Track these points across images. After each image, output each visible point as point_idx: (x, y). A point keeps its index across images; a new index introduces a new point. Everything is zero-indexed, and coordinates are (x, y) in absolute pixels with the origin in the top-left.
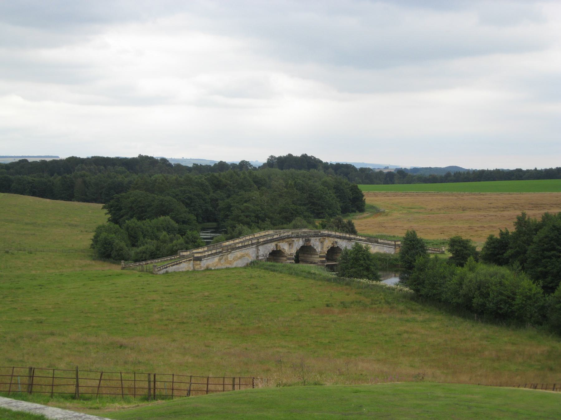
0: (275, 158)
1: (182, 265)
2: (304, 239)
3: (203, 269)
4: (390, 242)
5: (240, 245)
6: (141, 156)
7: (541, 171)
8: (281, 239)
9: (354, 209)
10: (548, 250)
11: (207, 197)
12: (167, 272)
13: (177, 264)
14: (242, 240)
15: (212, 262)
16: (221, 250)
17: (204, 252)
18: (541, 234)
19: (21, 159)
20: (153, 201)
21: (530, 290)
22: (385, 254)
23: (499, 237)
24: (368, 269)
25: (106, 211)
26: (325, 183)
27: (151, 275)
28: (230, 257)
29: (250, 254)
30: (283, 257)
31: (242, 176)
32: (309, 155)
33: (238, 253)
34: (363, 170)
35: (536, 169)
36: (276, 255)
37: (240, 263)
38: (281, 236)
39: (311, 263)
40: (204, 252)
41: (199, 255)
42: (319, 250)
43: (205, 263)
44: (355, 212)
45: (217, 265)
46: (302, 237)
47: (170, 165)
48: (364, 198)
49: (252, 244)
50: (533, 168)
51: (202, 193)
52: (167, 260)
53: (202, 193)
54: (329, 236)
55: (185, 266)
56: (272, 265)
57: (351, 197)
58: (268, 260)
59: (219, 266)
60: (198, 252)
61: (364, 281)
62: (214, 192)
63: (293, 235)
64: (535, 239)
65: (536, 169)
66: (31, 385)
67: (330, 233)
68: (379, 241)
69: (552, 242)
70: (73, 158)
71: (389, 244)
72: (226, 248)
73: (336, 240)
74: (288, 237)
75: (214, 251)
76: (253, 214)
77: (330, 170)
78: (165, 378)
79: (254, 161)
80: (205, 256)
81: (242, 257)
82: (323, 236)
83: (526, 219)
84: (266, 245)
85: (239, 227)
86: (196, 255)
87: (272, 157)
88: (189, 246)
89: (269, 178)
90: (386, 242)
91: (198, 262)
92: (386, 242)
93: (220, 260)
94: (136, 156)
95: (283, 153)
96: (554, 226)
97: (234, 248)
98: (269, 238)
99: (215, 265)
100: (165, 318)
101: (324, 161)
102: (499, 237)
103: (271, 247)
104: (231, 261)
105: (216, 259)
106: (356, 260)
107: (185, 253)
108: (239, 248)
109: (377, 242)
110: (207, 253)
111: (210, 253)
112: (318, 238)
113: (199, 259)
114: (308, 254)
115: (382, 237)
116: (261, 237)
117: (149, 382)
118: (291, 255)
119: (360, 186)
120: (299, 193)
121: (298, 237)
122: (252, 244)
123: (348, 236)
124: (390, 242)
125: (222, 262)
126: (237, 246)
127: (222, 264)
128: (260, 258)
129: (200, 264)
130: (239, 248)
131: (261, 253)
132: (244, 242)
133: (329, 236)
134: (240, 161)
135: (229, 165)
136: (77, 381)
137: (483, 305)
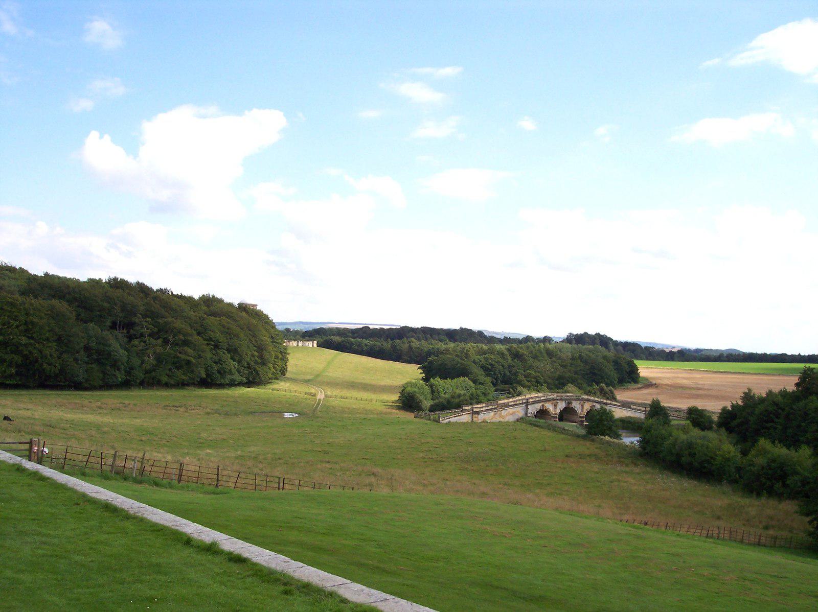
0: (573, 335)
1: (462, 417)
2: (567, 402)
3: (480, 421)
4: (641, 408)
5: (513, 403)
6: (461, 329)
7: (804, 356)
8: (547, 400)
9: (629, 380)
10: (767, 422)
11: (505, 364)
12: (449, 422)
13: (458, 416)
14: (515, 399)
15: (489, 416)
16: (496, 407)
17: (482, 407)
18: (761, 407)
19: (364, 326)
20: (457, 364)
21: (729, 453)
22: (630, 417)
23: (730, 409)
24: (610, 428)
25: (421, 371)
26: (605, 358)
27: (436, 423)
28: (504, 413)
29: (519, 412)
30: (549, 415)
31: (537, 348)
32: (602, 333)
33: (510, 410)
34: (647, 348)
35: (799, 354)
36: (542, 413)
37: (511, 419)
38: (548, 397)
39: (573, 422)
40: (482, 407)
41: (478, 410)
42: (579, 411)
43: (481, 417)
44: (630, 383)
45: (492, 419)
46: (565, 400)
47: (485, 337)
48: (639, 371)
49: (523, 403)
50: (797, 354)
51: (501, 360)
52: (451, 412)
53: (501, 360)
54: (588, 400)
55: (465, 418)
56: (537, 421)
57: (628, 370)
58: (536, 416)
59: (494, 420)
60: (477, 407)
61: (607, 438)
62: (512, 360)
63: (558, 398)
64: (757, 411)
65: (799, 354)
66: (180, 475)
67: (589, 398)
68: (632, 406)
69: (771, 415)
70: (406, 327)
71: (640, 410)
72: (500, 405)
73: (594, 404)
74: (553, 399)
75: (490, 407)
76: (535, 380)
77: (620, 348)
78: (192, 468)
79: (155, 288)
80: (482, 411)
81: (513, 414)
82: (583, 400)
83: (752, 394)
84: (534, 405)
85: (520, 389)
86: (475, 410)
87: (570, 334)
88: (473, 402)
89: (560, 350)
90: (638, 408)
91: (476, 415)
92: (638, 408)
93: (495, 414)
94: (458, 328)
95: (580, 331)
96: (774, 402)
97: (507, 406)
98: (537, 399)
99: (490, 418)
100: (427, 457)
101: (614, 339)
102: (730, 409)
103: (538, 406)
104: (504, 416)
105: (492, 414)
106: (601, 420)
107: (466, 408)
108: (511, 406)
109: (631, 408)
110: (484, 409)
111: (486, 408)
112: (579, 402)
113: (478, 413)
114: (570, 414)
115: (633, 403)
116: (531, 398)
117: (279, 483)
118: (555, 414)
119: (636, 362)
120: (582, 364)
121: (561, 400)
122: (523, 403)
123: (605, 401)
124: (641, 408)
125: (497, 416)
126: (510, 404)
127: (496, 418)
128: (529, 415)
129: (477, 417)
130: (511, 406)
131: (530, 411)
132: (516, 401)
133: (588, 400)
134: (544, 336)
135: (534, 339)
136: (218, 476)
137: (691, 464)
